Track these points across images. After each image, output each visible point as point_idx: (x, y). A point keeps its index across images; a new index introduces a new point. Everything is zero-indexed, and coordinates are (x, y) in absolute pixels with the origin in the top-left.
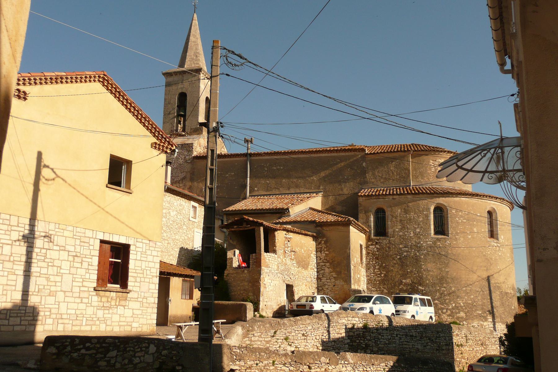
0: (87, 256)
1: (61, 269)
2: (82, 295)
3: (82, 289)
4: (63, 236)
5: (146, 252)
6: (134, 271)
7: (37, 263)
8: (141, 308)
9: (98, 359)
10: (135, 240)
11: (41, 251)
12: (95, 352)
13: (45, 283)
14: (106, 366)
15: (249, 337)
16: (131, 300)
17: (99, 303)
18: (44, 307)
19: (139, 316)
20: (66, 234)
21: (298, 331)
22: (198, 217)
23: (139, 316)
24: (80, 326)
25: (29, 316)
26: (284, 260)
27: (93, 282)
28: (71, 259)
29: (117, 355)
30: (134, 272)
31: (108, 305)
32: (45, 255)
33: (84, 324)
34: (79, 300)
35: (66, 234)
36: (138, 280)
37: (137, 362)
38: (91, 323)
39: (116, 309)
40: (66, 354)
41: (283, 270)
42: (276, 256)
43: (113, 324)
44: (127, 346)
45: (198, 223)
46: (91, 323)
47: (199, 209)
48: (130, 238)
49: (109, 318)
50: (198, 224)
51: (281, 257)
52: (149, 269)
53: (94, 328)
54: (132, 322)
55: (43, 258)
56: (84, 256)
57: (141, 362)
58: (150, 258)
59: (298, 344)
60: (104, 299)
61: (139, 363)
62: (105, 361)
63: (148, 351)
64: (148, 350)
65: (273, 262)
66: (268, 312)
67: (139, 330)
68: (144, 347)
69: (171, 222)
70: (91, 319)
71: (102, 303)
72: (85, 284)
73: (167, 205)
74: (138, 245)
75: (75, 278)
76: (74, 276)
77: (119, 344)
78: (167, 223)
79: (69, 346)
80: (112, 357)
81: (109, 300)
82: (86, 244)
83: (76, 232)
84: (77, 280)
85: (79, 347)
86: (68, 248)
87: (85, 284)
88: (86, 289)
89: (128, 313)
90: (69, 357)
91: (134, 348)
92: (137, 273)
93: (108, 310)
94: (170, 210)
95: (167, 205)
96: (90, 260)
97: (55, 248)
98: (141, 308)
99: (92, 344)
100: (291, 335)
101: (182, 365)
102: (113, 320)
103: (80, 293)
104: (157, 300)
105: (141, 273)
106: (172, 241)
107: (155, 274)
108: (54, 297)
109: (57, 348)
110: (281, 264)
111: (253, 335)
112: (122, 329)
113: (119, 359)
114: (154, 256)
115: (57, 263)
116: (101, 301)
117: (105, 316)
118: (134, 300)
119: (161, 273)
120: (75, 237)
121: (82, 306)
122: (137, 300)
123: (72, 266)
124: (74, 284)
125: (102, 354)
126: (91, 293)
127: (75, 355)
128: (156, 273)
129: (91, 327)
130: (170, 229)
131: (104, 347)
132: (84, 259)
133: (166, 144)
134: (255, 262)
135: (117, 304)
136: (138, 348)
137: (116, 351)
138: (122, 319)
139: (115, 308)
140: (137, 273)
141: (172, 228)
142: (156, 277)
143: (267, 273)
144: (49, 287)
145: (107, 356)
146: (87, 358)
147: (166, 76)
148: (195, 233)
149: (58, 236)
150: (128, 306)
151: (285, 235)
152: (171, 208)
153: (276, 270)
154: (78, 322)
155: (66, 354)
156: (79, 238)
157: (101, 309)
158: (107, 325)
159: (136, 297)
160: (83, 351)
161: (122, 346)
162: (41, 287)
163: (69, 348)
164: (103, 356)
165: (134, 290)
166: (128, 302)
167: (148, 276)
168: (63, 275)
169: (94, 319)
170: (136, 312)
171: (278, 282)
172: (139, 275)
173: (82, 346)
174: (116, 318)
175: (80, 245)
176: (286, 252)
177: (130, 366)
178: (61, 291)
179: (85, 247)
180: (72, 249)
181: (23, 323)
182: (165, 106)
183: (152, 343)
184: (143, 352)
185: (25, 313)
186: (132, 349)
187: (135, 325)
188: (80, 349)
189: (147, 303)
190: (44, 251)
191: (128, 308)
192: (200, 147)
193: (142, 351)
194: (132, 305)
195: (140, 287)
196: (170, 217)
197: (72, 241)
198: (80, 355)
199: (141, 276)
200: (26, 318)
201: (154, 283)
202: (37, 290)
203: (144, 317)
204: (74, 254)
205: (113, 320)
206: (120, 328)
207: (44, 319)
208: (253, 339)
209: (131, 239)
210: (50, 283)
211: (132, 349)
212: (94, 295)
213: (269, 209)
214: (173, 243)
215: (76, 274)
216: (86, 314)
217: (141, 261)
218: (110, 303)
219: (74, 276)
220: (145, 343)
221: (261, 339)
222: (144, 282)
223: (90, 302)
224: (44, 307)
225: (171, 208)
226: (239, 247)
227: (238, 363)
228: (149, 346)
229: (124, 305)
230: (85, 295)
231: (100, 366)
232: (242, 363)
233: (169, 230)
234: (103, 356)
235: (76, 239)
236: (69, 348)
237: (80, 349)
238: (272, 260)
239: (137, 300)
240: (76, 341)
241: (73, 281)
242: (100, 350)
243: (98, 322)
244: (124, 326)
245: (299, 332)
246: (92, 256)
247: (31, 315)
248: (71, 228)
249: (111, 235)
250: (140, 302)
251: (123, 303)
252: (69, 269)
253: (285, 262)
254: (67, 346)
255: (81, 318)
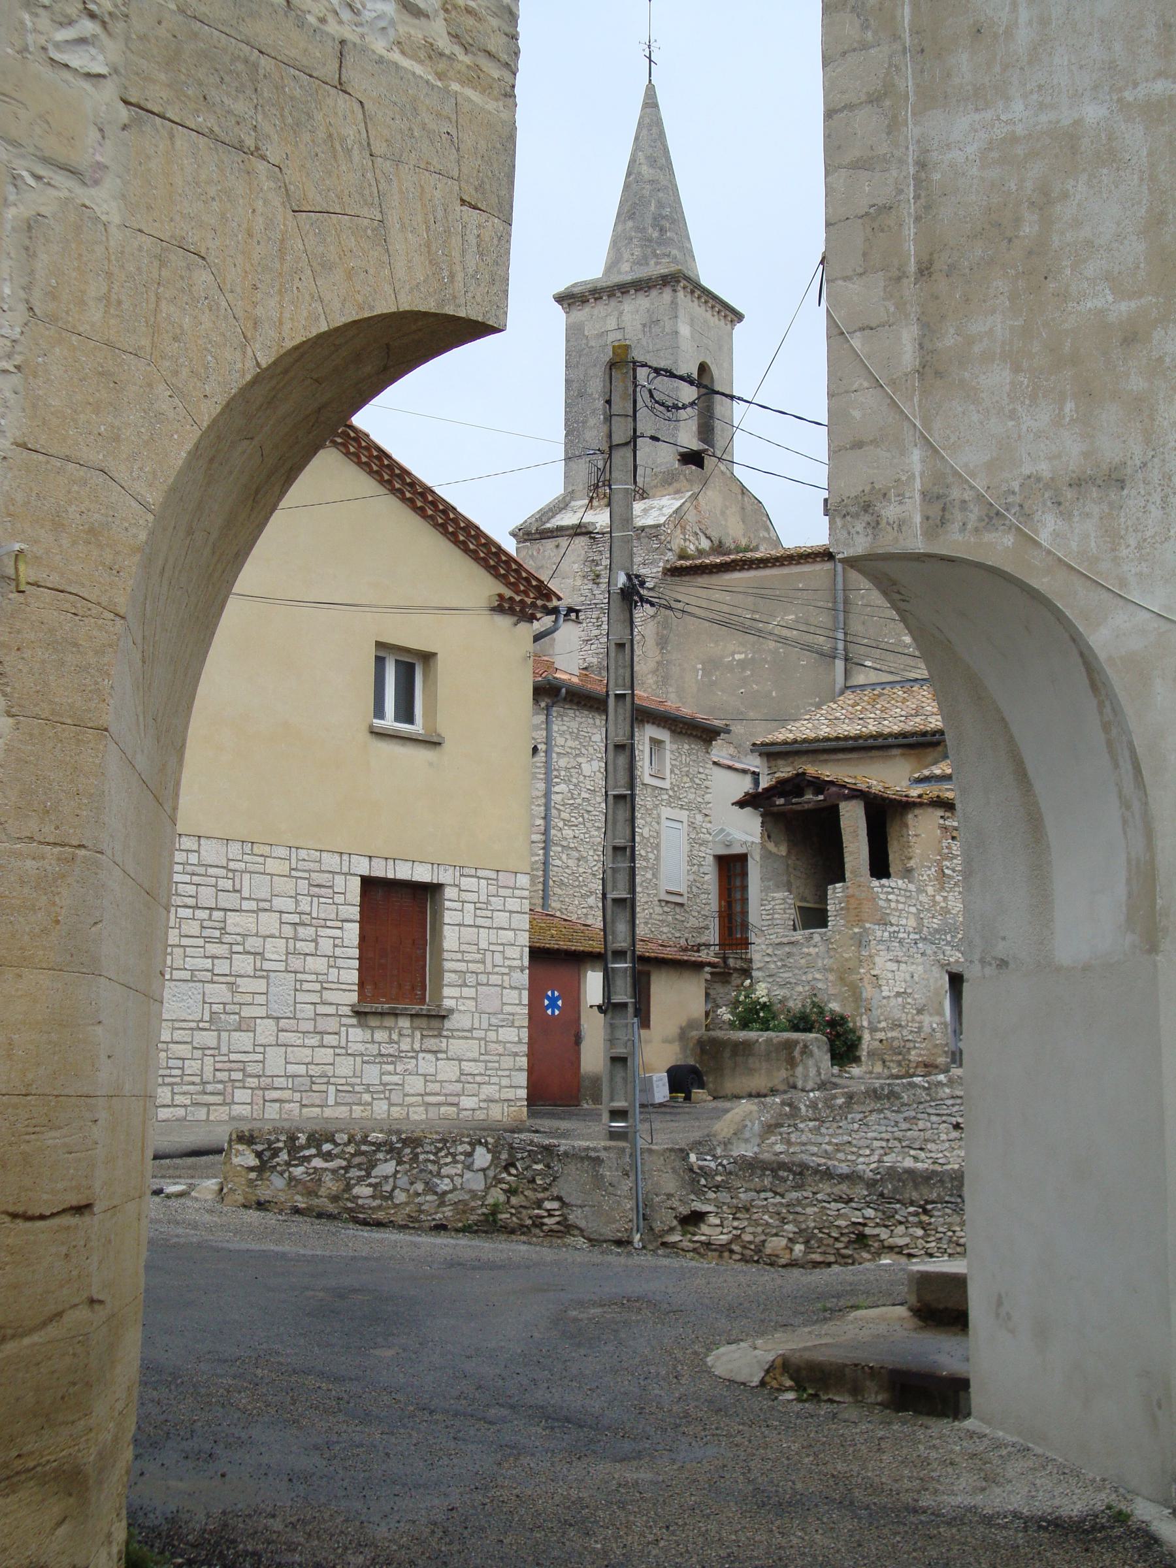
0: (329, 923)
1: (264, 959)
2: (322, 1024)
3: (322, 1009)
4: (264, 874)
5: (488, 903)
6: (459, 956)
7: (203, 947)
8: (482, 1058)
9: (353, 1182)
10: (457, 874)
11: (211, 915)
12: (344, 1163)
13: (227, 997)
14: (373, 1197)
15: (781, 1134)
16: (453, 1037)
17: (368, 1046)
18: (226, 1058)
19: (478, 1079)
20: (272, 866)
21: (938, 1115)
22: (672, 772)
23: (478, 1079)
24: (321, 1106)
25: (193, 1083)
26: (938, 898)
27: (350, 990)
28: (288, 931)
29: (397, 1172)
30: (459, 960)
31: (391, 1051)
32: (222, 925)
33: (331, 1101)
34: (314, 1041)
35: (272, 866)
36: (471, 980)
37: (446, 1188)
38: (349, 1098)
39: (414, 1061)
40: (279, 1168)
41: (937, 931)
42: (912, 887)
43: (409, 1100)
44: (419, 1150)
45: (672, 789)
46: (349, 1098)
47: (675, 747)
48: (442, 868)
49: (397, 1084)
50: (671, 793)
51: (930, 890)
52: (500, 948)
53: (357, 1111)
54: (458, 1095)
55: (217, 933)
56: (322, 922)
57: (455, 1189)
58: (501, 919)
59: (940, 1155)
60: (380, 1035)
61: (451, 1191)
62: (370, 1185)
63: (473, 1163)
64: (470, 1160)
65: (901, 906)
66: (892, 1061)
67: (480, 1115)
68: (461, 1154)
69: (584, 795)
70: (349, 1088)
71: (376, 1046)
72: (328, 995)
73: (570, 743)
74: (466, 883)
75: (301, 981)
76: (299, 976)
77: (399, 1145)
78: (573, 798)
79: (285, 1151)
80: (386, 1178)
81: (395, 1037)
82: (323, 891)
83: (298, 860)
84: (306, 986)
85: (307, 1153)
86: (278, 903)
87: (328, 995)
88: (331, 1010)
89: (449, 1070)
90: (286, 1175)
91: (435, 1154)
92: (467, 962)
93: (392, 1063)
94: (580, 760)
95: (570, 743)
96: (338, 933)
97: (246, 905)
98: (482, 1058)
99: (336, 1145)
100: (915, 1127)
101: (559, 1199)
102: (408, 1089)
103: (315, 1020)
104: (525, 1034)
105: (478, 962)
106: (591, 853)
107: (517, 963)
108: (251, 1034)
109: (259, 1155)
110: (928, 910)
111: (795, 1126)
112: (433, 1113)
113: (403, 1181)
114: (511, 912)
115: (253, 943)
116: (373, 1042)
117: (386, 1078)
118: (461, 1034)
119: (540, 955)
120: (294, 873)
121: (325, 1055)
122: (469, 1035)
123: (291, 950)
124: (301, 997)
125: (361, 1170)
126: (345, 1020)
127: (298, 1171)
128: (521, 959)
129: (351, 1110)
130: (583, 816)
131: (363, 1153)
132: (322, 931)
133: (532, 595)
134: (842, 909)
135: (417, 1046)
136: (446, 1156)
137: (394, 1163)
138: (435, 1087)
139: (412, 1057)
140: (467, 962)
141: (588, 812)
142: (522, 971)
143: (881, 941)
144: (236, 1008)
145: (374, 1173)
146: (327, 1178)
147: (566, 306)
148: (664, 823)
149: (251, 872)
150: (446, 1052)
151: (941, 821)
152: (583, 751)
153: (911, 930)
154: (316, 1098)
155: (279, 1168)
156: (306, 875)
157: (374, 1063)
158: (391, 1105)
159: (468, 1026)
160: (317, 1163)
161: (408, 1150)
162: (215, 1008)
163: (284, 1156)
164: (363, 1173)
165: (462, 1008)
166: (444, 1040)
167: (497, 969)
168: (271, 974)
169: (357, 1088)
170: (468, 1067)
171: (920, 968)
172: (472, 967)
173: (313, 1151)
174: (415, 1084)
175: (308, 895)
176: (946, 871)
177: (428, 1198)
178: (268, 1017)
179: (322, 900)
180: (289, 904)
181: (179, 1099)
182: (567, 405)
183: (480, 1143)
184: (460, 1166)
185: (183, 1074)
186: (432, 1157)
187: (467, 1102)
188: (308, 1159)
189: (498, 1042)
190: (218, 915)
191: (448, 1059)
192: (685, 535)
193: (455, 1162)
194: (456, 1046)
195: (475, 999)
196: (581, 778)
197: (286, 885)
198: (311, 1171)
199: (478, 967)
200: (185, 1088)
201: (516, 988)
202: (207, 1017)
203: (494, 1080)
204: (296, 919)
205: (408, 1089)
206: (426, 1111)
207: (229, 1090)
208: (793, 1138)
209: (446, 870)
210: (238, 998)
211: (432, 1157)
212: (352, 1026)
213: (903, 735)
214: (596, 858)
215: (304, 972)
216: (334, 1076)
217: (476, 930)
218: (396, 1046)
219: (299, 976)
220: (462, 1143)
221: (819, 1139)
222: (487, 985)
223: (343, 1044)
224: (226, 1058)
225: (583, 751)
226: (799, 863)
227: (711, 1195)
228: (474, 1150)
229: (435, 1049)
230: (332, 1024)
231: (359, 1197)
232: (724, 1196)
233: (581, 819)
234: (363, 1173)
235: (297, 878)
236: (284, 1156)
237: (308, 1159)
238: (897, 901)
239: (469, 1035)
240: (298, 1138)
241: (296, 990)
242: (357, 1160)
243: (367, 1097)
244: (439, 1104)
245: (944, 1118)
246: (343, 921)
247: (197, 1079)
248: (282, 852)
249: (391, 862)
250: (480, 1039)
251: (431, 1043)
252: (284, 958)
253: (943, 904)
254: (281, 1149)
255: (324, 1088)
